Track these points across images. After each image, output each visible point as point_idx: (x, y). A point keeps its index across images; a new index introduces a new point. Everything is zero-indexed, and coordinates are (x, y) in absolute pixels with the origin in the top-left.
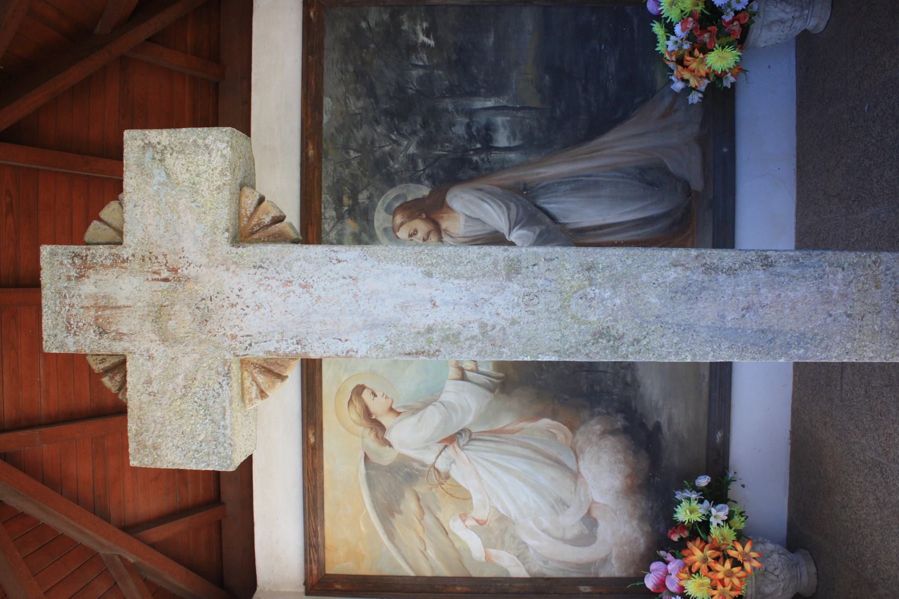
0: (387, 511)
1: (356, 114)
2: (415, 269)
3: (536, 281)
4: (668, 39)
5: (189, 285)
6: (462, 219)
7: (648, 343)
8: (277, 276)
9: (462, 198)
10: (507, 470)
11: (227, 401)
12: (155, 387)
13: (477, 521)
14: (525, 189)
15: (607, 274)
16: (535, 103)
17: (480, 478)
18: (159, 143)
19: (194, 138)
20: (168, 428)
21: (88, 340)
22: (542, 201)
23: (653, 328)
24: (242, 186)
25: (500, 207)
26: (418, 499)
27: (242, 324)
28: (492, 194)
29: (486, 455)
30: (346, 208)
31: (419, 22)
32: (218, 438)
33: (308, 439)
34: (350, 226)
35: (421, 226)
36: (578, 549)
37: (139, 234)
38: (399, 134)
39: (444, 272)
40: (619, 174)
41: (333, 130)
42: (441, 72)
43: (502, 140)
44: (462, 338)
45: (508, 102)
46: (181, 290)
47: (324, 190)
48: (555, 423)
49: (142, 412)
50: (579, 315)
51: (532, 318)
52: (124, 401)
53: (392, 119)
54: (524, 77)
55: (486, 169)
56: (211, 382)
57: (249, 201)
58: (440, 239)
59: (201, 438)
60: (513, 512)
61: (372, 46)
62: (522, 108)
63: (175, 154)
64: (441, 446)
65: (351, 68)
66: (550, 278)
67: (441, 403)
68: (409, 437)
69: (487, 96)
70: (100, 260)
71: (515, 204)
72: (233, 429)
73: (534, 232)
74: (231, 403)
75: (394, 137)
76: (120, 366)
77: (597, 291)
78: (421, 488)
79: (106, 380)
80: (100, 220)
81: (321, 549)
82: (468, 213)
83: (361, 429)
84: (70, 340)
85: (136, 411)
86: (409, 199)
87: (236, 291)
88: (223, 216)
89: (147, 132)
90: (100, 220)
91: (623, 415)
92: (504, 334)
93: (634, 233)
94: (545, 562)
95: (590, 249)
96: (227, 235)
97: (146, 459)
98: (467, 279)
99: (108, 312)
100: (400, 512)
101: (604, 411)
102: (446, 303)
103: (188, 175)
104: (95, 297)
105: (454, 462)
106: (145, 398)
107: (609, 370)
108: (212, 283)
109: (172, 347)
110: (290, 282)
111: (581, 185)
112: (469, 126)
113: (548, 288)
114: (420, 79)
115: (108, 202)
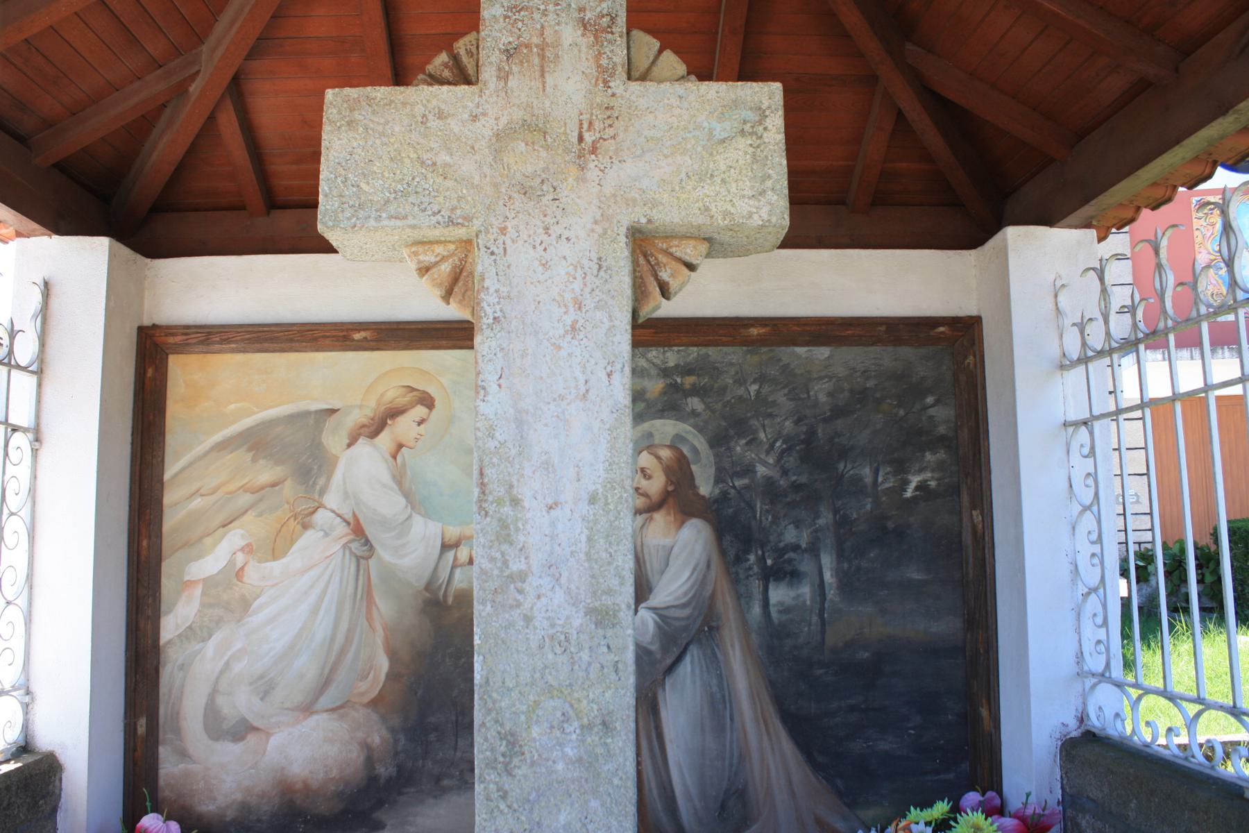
0: (257, 441)
1: (808, 393)
2: (600, 481)
3: (587, 651)
4: (928, 824)
5: (574, 171)
6: (668, 541)
7: (501, 812)
8: (587, 290)
9: (696, 541)
10: (314, 612)
11: (414, 222)
12: (434, 123)
13: (242, 568)
14: (711, 628)
15: (599, 750)
16: (830, 639)
17: (303, 572)
18: (765, 129)
19: (774, 176)
20: (378, 141)
21: (498, 34)
22: (695, 652)
23: (523, 818)
24: (709, 240)
25: (686, 594)
26: (274, 485)
27: (521, 243)
28: (703, 582)
29: (336, 579)
30: (679, 380)
31: (936, 475)
32: (363, 209)
33: (359, 331)
34: (655, 386)
35: (656, 485)
36: (200, 713)
37: (642, 103)
38: (783, 452)
39: (596, 521)
40: (735, 760)
41: (785, 360)
42: (869, 507)
43: (779, 594)
44: (504, 547)
45: (831, 601)
46: (567, 158)
47: (703, 350)
48: (383, 677)
49: (399, 106)
50: (540, 712)
51: (534, 645)
52: (415, 82)
53: (803, 442)
54: (866, 623)
55: (737, 573)
56: (441, 199)
57: (689, 251)
58: (638, 512)
59: (363, 186)
60: (255, 620)
61: (902, 412)
62: (823, 621)
63: (751, 150)
64: (349, 517)
65: (870, 384)
66: (591, 669)
67: (410, 517)
68: (361, 471)
69: (838, 572)
70: (607, 50)
71: (691, 614)
72: (376, 229)
73: (651, 643)
74: (413, 227)
75: (778, 444)
76: (463, 77)
77: (574, 737)
78: (289, 489)
79: (443, 57)
80: (660, 51)
81: (204, 348)
82: (675, 550)
83: (373, 404)
84: (498, 11)
85: (401, 97)
86: (694, 467)
87: (566, 234)
88: (669, 215)
89: (781, 113)
90: (660, 51)
91: (394, 774)
92: (511, 607)
93: (653, 785)
94: (182, 667)
95: (633, 725)
96: (643, 220)
97: (335, 111)
98: (587, 554)
99: (536, 61)
100: (254, 460)
101: (400, 748)
102: (553, 524)
103: (723, 167)
104: (557, 44)
105: (326, 535)
106: (419, 110)
107: (459, 754)
108: (578, 201)
109: (489, 147)
110: (580, 308)
111: (719, 706)
112: (796, 548)
113: (576, 667)
114: (858, 480)
115: (685, 61)
